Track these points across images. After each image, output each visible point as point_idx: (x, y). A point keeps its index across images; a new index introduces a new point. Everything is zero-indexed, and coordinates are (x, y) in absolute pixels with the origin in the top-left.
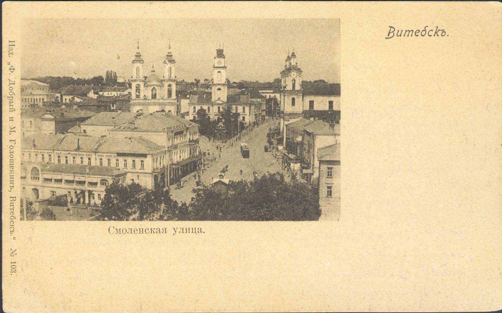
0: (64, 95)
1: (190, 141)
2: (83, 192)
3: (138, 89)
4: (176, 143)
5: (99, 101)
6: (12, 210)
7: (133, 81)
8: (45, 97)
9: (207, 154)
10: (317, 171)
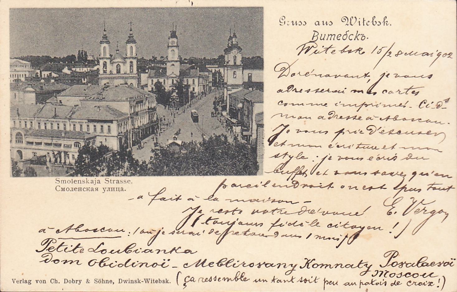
0: (43, 71)
1: (149, 109)
2: (60, 153)
3: (105, 65)
4: (137, 111)
5: (72, 76)
7: (100, 59)
8: (27, 74)
9: (163, 119)
10: (254, 132)
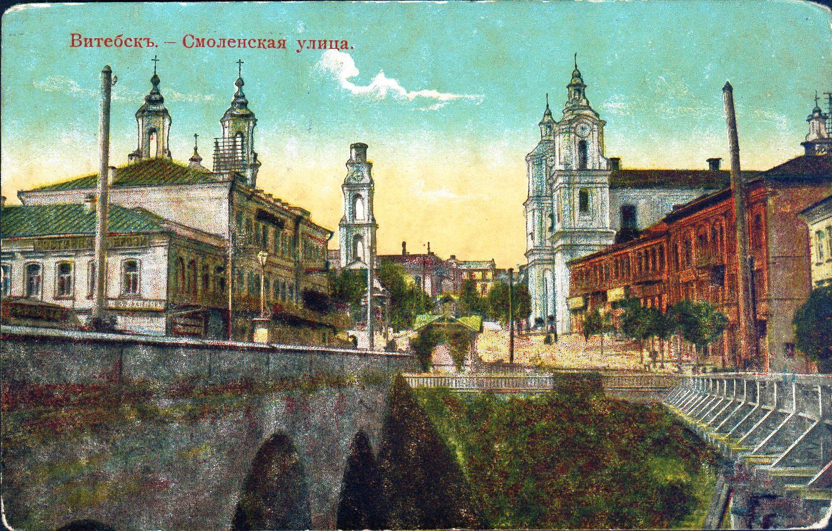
6: (102, 43)
